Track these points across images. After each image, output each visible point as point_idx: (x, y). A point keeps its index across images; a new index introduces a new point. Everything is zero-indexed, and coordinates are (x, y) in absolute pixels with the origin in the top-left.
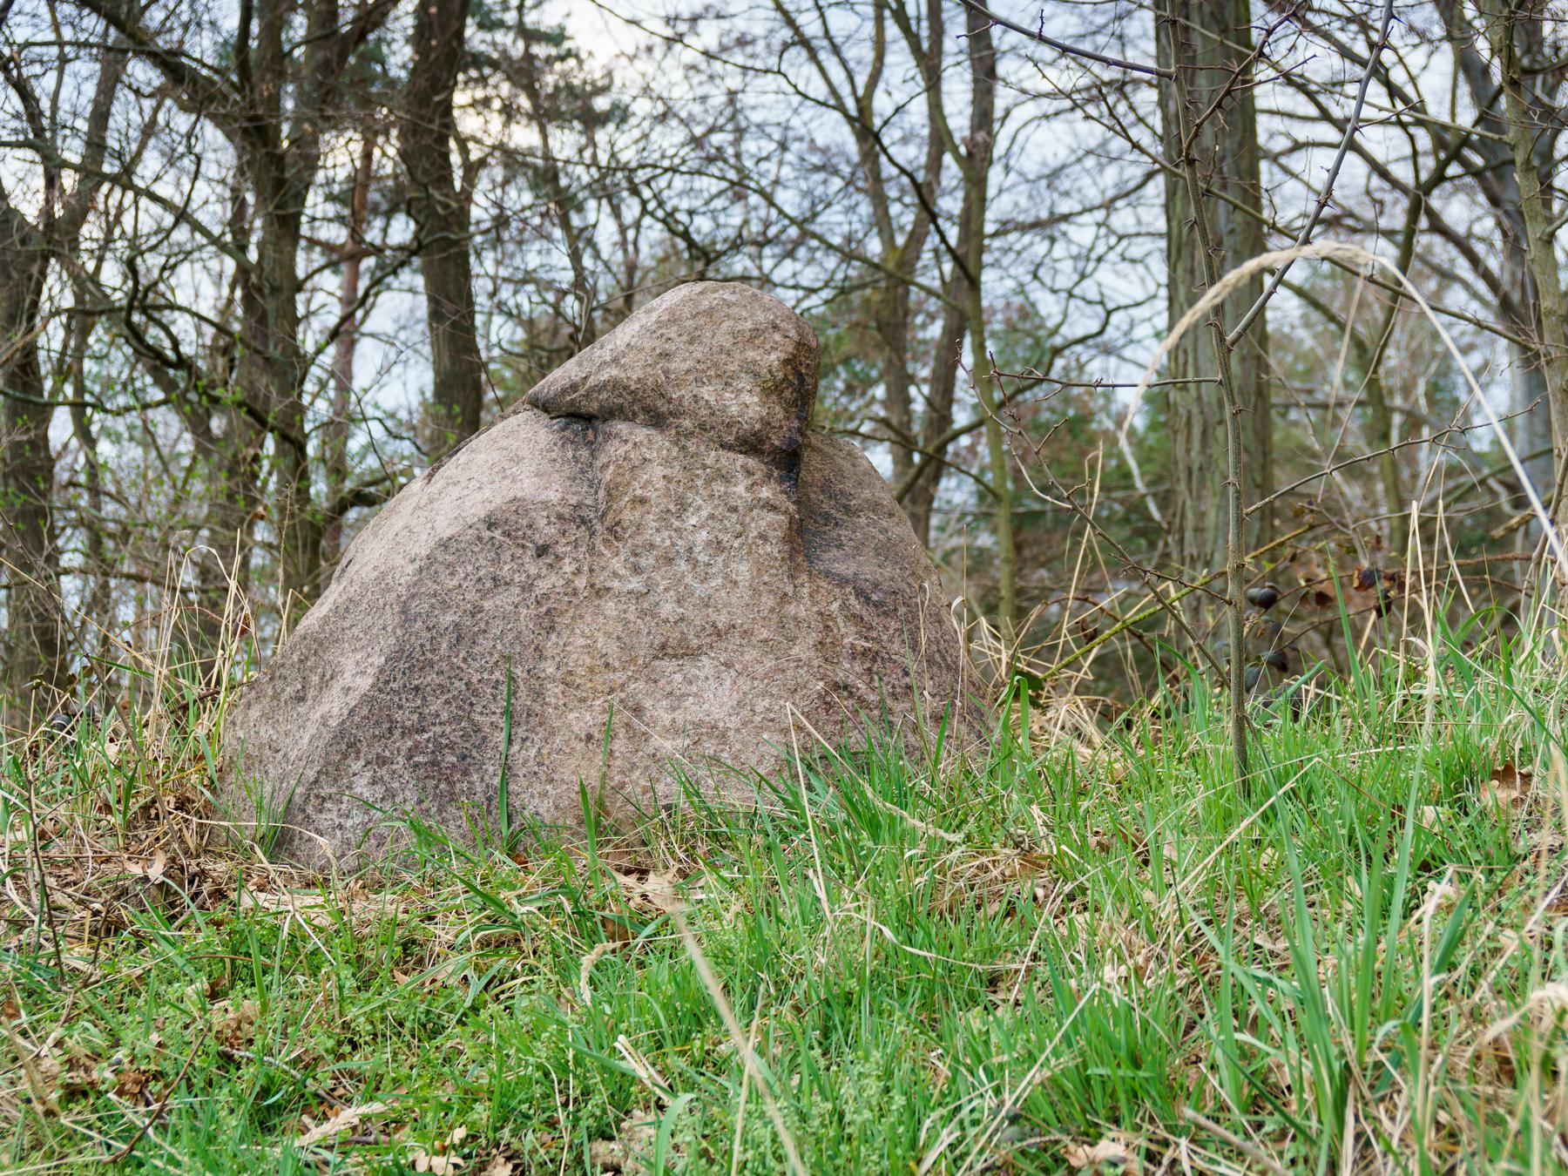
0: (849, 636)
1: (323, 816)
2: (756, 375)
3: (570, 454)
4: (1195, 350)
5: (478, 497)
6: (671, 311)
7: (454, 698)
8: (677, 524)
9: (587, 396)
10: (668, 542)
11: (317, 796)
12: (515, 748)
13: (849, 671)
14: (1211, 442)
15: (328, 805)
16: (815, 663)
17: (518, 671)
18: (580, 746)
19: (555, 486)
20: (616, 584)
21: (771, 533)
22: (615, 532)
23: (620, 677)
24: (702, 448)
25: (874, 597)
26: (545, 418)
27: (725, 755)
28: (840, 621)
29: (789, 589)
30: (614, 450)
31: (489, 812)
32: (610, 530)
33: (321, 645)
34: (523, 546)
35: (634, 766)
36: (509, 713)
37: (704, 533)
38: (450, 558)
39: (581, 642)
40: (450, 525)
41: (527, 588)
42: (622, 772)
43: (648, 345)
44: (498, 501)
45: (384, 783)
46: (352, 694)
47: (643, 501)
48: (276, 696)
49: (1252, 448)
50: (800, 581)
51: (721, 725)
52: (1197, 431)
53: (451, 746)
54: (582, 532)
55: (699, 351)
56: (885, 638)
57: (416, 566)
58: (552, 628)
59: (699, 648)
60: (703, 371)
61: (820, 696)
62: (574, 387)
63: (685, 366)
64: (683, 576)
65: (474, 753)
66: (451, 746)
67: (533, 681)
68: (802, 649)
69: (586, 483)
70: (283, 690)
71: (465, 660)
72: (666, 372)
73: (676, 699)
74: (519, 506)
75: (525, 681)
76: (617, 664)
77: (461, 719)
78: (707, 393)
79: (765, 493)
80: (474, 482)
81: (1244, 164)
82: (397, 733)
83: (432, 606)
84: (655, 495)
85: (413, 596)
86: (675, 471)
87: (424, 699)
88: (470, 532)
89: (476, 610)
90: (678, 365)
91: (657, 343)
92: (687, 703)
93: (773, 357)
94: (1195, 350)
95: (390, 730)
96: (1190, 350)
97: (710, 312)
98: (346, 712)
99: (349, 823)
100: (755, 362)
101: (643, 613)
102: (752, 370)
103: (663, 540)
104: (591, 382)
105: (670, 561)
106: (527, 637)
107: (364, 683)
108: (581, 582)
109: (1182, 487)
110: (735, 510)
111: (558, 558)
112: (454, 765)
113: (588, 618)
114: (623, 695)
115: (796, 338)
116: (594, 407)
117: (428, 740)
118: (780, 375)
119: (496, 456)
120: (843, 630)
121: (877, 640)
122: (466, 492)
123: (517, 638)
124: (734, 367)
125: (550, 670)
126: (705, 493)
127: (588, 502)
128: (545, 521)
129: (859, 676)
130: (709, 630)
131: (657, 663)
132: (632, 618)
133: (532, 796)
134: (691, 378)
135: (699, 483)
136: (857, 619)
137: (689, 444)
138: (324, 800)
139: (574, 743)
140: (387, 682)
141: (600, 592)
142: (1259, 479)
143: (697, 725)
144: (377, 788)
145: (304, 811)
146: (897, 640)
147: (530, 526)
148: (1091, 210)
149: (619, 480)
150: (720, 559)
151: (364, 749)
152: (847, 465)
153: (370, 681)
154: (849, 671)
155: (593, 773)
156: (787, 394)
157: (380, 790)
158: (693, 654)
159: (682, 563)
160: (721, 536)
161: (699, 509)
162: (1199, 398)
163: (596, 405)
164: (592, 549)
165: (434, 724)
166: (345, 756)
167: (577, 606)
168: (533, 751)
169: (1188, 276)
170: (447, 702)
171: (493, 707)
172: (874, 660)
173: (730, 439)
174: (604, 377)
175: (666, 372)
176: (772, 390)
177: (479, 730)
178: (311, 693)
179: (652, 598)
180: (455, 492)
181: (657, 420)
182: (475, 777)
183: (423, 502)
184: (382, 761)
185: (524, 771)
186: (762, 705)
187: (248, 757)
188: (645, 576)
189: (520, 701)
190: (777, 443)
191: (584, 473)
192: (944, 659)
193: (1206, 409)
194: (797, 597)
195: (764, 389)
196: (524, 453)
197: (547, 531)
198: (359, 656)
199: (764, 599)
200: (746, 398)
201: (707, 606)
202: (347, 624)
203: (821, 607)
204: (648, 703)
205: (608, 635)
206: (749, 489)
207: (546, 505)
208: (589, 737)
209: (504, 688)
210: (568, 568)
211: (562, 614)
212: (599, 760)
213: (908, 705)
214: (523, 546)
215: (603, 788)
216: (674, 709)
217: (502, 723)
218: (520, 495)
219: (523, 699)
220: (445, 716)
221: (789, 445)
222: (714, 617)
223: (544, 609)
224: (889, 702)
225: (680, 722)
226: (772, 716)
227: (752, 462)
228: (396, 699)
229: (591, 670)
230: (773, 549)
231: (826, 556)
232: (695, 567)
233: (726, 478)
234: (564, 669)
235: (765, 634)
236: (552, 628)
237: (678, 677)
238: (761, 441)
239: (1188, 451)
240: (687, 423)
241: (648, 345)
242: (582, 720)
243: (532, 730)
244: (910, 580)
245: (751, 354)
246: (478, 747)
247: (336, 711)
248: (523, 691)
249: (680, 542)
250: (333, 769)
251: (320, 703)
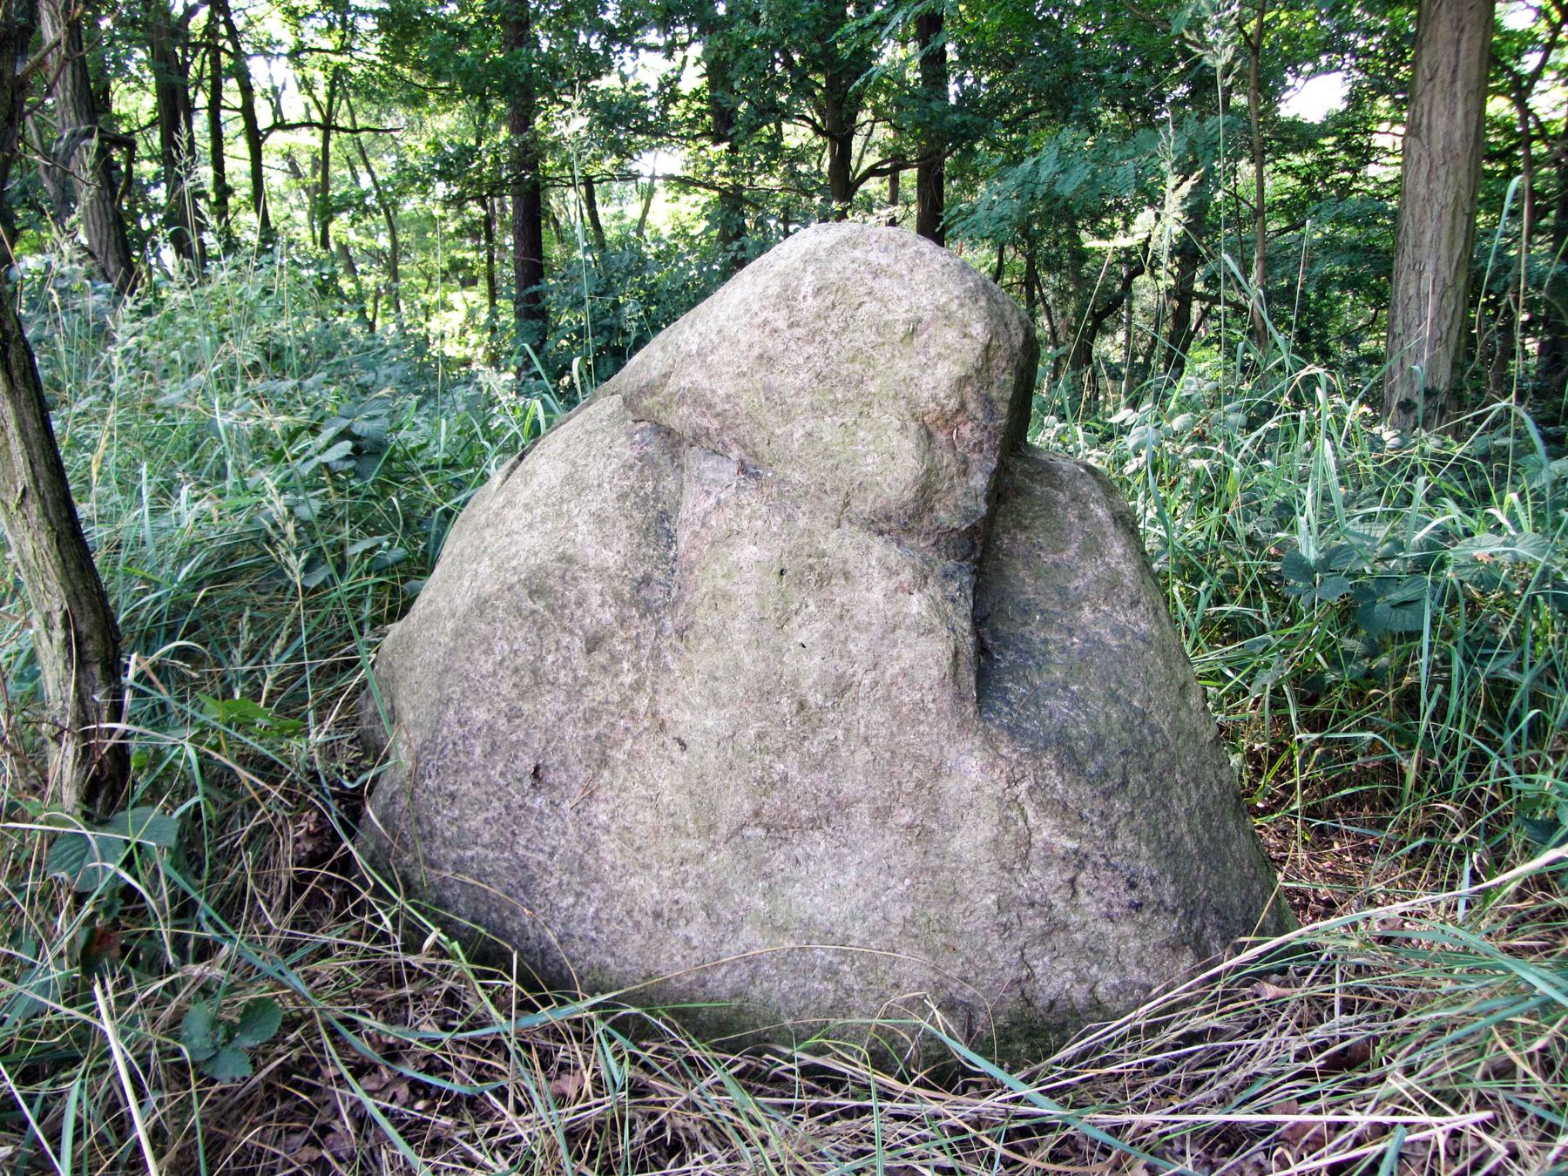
79: (916, 605)
111: (615, 659)
114: (701, 869)
148: (1459, 40)
164: (656, 655)
172: (1081, 866)
210: (628, 679)
218: (570, 552)
220: (486, 838)
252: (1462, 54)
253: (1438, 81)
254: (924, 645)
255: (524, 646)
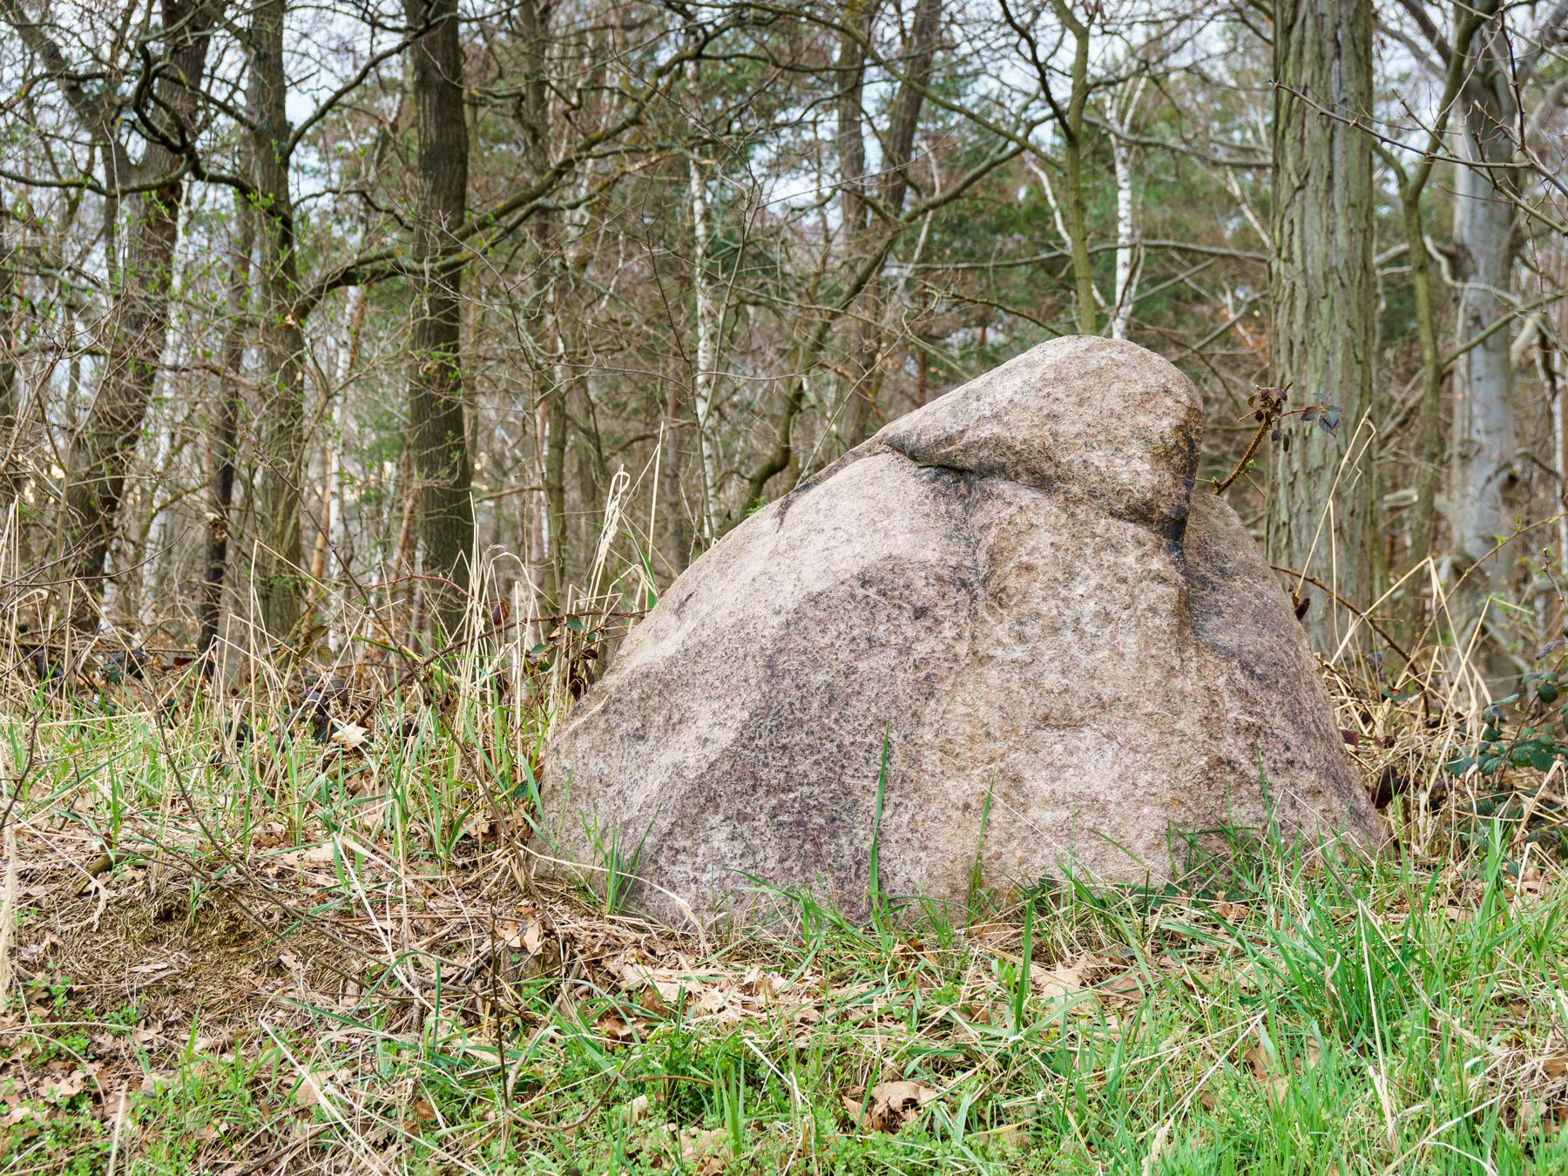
0: (1234, 710)
1: (677, 868)
2: (1148, 441)
3: (943, 508)
4: (1302, 222)
5: (848, 550)
6: (1056, 368)
7: (824, 759)
8: (1064, 593)
9: (965, 451)
10: (1055, 612)
11: (671, 848)
12: (888, 813)
13: (1232, 747)
14: (1314, 315)
15: (682, 857)
16: (1200, 738)
17: (894, 735)
18: (957, 815)
19: (932, 545)
20: (999, 652)
21: (1162, 607)
22: (999, 598)
23: (1000, 747)
24: (1092, 516)
25: (1258, 671)
26: (911, 467)
27: (1104, 827)
28: (1226, 695)
29: (1176, 663)
30: (995, 511)
31: (858, 876)
32: (994, 596)
33: (667, 685)
34: (900, 607)
35: (1011, 836)
36: (882, 776)
37: (1092, 604)
38: (821, 615)
39: (961, 710)
40: (818, 578)
41: (905, 650)
42: (999, 843)
43: (1033, 404)
44: (871, 558)
45: (744, 840)
46: (710, 747)
47: (1029, 568)
48: (609, 730)
49: (1355, 325)
50: (1187, 655)
51: (1102, 797)
52: (1300, 304)
53: (820, 808)
54: (963, 596)
55: (1089, 414)
56: (1268, 712)
57: (783, 618)
58: (932, 694)
59: (1082, 719)
60: (1094, 436)
61: (1203, 772)
62: (950, 440)
63: (1075, 429)
64: (1069, 647)
65: (844, 816)
66: (820, 808)
67: (909, 747)
68: (1188, 723)
69: (963, 543)
70: (618, 725)
71: (837, 721)
72: (1055, 435)
73: (1057, 770)
74: (896, 564)
75: (901, 746)
76: (998, 734)
77: (831, 780)
78: (1097, 458)
80: (840, 533)
81: (1360, 32)
82: (761, 791)
83: (802, 663)
84: (1041, 562)
85: (780, 651)
86: (1064, 539)
87: (792, 758)
88: (842, 588)
89: (850, 671)
90: (1067, 428)
91: (1044, 402)
92: (1067, 775)
93: (1165, 423)
94: (1302, 222)
95: (754, 787)
96: (1296, 221)
97: (1099, 372)
98: (705, 766)
99: (705, 877)
100: (1146, 428)
101: (1027, 683)
102: (1143, 436)
103: (1050, 610)
104: (969, 436)
105: (1056, 630)
106: (905, 702)
107: (726, 737)
108: (962, 648)
109: (1283, 359)
110: (1124, 581)
112: (821, 827)
113: (970, 686)
114: (1002, 765)
115: (1188, 403)
116: (972, 462)
117: (795, 800)
118: (1172, 442)
119: (862, 505)
120: (1228, 705)
121: (1261, 715)
122: (832, 543)
123: (894, 702)
124: (1125, 432)
125: (928, 737)
126: (1094, 562)
127: (968, 563)
128: (923, 582)
129: (1242, 751)
130: (1094, 702)
131: (1038, 733)
132: (1015, 688)
133: (904, 863)
134: (1081, 442)
135: (1088, 551)
136: (1242, 693)
137: (1078, 511)
138: (678, 852)
139: (950, 812)
140: (753, 739)
141: (982, 660)
142: (1361, 355)
143: (1078, 797)
144: (736, 843)
145: (656, 862)
146: (1278, 714)
147: (907, 587)
149: (1003, 544)
150: (1107, 630)
151: (724, 804)
152: (1220, 524)
153: (732, 735)
154: (1232, 747)
155: (969, 842)
156: (1176, 460)
157: (739, 847)
158: (1074, 725)
159: (1069, 633)
160: (1109, 607)
161: (1087, 578)
162: (1305, 270)
163: (974, 461)
164: (973, 615)
165: (801, 784)
166: (703, 810)
167: (958, 673)
168: (906, 818)
169: (1297, 145)
170: (817, 763)
171: (865, 770)
173: (1120, 507)
174: (985, 432)
175: (1055, 435)
176: (1162, 456)
177: (850, 793)
178: (653, 733)
179: (1035, 668)
180: (820, 541)
181: (1042, 483)
182: (844, 840)
183: (781, 549)
184: (742, 817)
185: (896, 836)
186: (1144, 778)
187: (575, 788)
188: (1030, 645)
189: (895, 766)
190: (1166, 511)
191: (958, 531)
192: (1318, 728)
193: (1311, 282)
194: (1184, 671)
195: (1154, 455)
196: (894, 504)
197: (926, 593)
198: (715, 705)
199: (1150, 672)
200: (1137, 464)
201: (1092, 677)
202: (699, 668)
203: (1208, 682)
204: (1027, 774)
205: (990, 704)
206: (1140, 559)
207: (923, 565)
208: (967, 807)
209: (879, 753)
211: (942, 680)
212: (976, 830)
213: (1287, 780)
214: (900, 607)
215: (979, 858)
216: (1053, 780)
217: (875, 787)
218: (895, 552)
219: (898, 763)
220: (813, 777)
221: (1178, 514)
222: (1099, 689)
223: (923, 675)
224: (1270, 778)
225: (1060, 794)
226: (1154, 790)
227: (1142, 532)
228: (762, 756)
229: (972, 739)
230: (1163, 622)
231: (1209, 626)
232: (1081, 638)
233: (1116, 548)
234: (943, 737)
235: (1150, 708)
236: (932, 694)
237: (1059, 748)
238: (1151, 510)
239: (1290, 324)
240: (1076, 489)
241: (1033, 404)
242: (959, 788)
243: (907, 796)
244: (1287, 648)
245: (1142, 419)
246: (849, 810)
247: (691, 762)
248: (897, 757)
249: (1067, 612)
250: (688, 822)
251: (666, 746)
252: (1337, 157)
253: (1309, 190)
254: (1161, 589)
255: (858, 622)
